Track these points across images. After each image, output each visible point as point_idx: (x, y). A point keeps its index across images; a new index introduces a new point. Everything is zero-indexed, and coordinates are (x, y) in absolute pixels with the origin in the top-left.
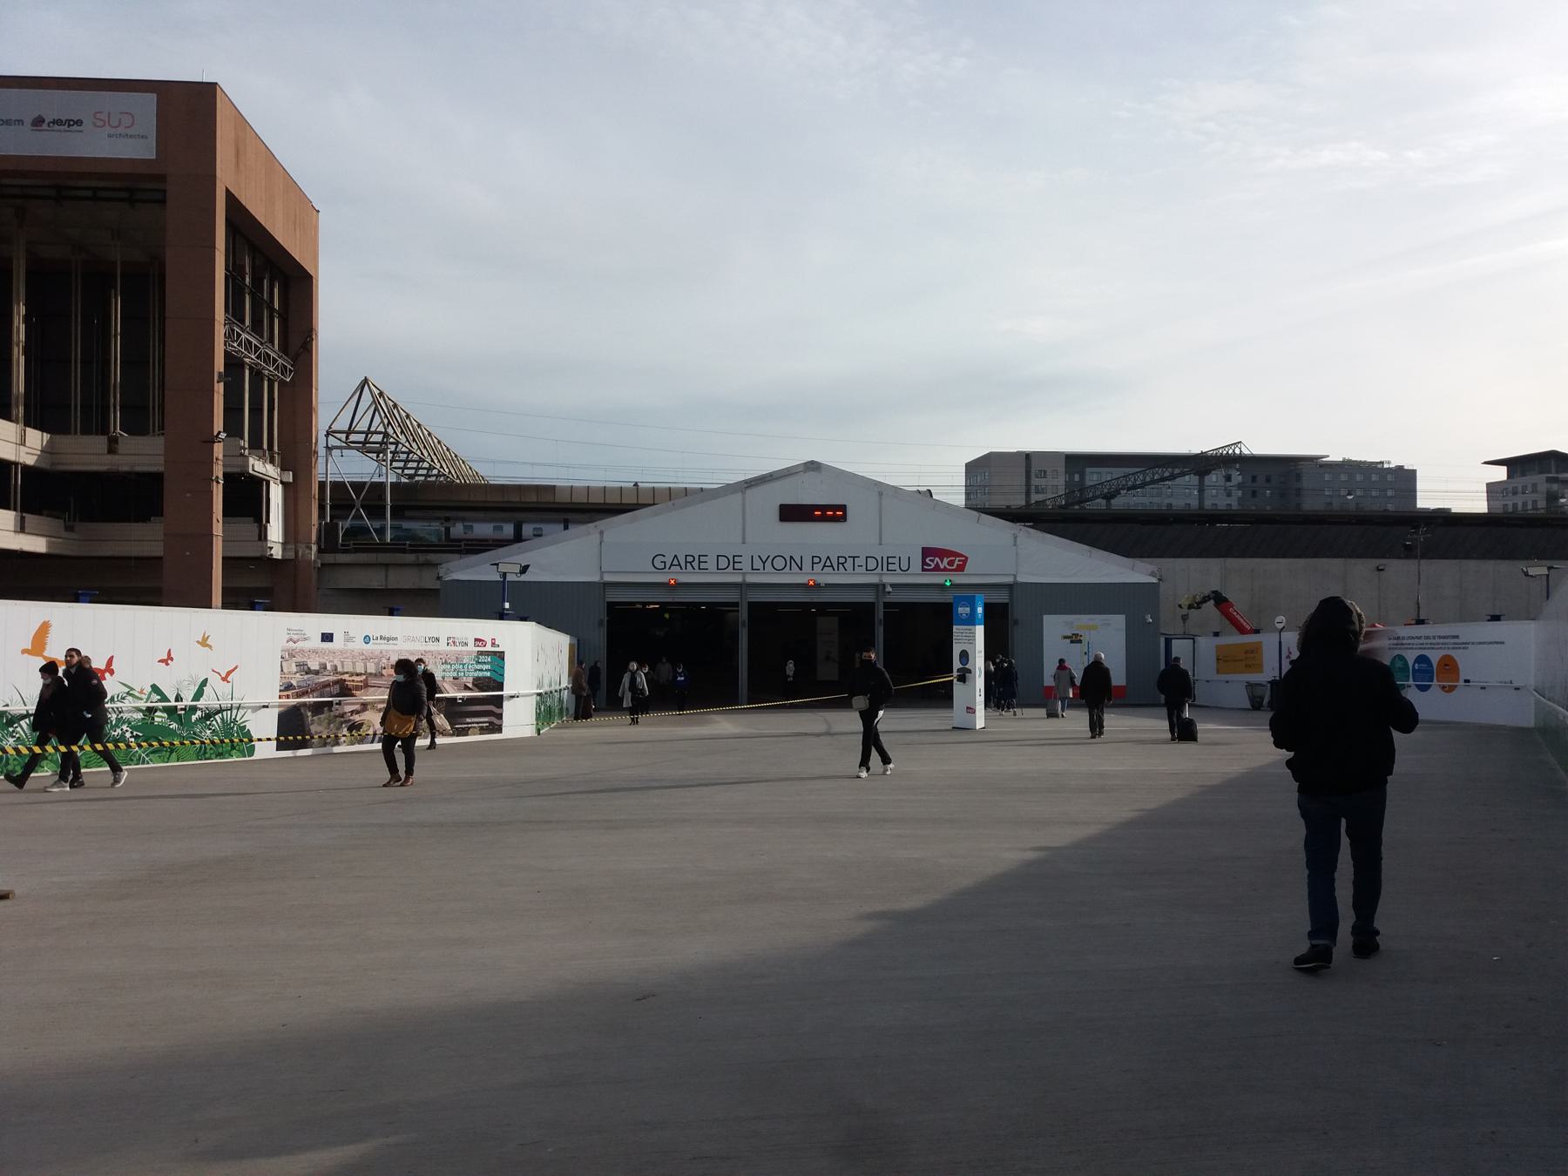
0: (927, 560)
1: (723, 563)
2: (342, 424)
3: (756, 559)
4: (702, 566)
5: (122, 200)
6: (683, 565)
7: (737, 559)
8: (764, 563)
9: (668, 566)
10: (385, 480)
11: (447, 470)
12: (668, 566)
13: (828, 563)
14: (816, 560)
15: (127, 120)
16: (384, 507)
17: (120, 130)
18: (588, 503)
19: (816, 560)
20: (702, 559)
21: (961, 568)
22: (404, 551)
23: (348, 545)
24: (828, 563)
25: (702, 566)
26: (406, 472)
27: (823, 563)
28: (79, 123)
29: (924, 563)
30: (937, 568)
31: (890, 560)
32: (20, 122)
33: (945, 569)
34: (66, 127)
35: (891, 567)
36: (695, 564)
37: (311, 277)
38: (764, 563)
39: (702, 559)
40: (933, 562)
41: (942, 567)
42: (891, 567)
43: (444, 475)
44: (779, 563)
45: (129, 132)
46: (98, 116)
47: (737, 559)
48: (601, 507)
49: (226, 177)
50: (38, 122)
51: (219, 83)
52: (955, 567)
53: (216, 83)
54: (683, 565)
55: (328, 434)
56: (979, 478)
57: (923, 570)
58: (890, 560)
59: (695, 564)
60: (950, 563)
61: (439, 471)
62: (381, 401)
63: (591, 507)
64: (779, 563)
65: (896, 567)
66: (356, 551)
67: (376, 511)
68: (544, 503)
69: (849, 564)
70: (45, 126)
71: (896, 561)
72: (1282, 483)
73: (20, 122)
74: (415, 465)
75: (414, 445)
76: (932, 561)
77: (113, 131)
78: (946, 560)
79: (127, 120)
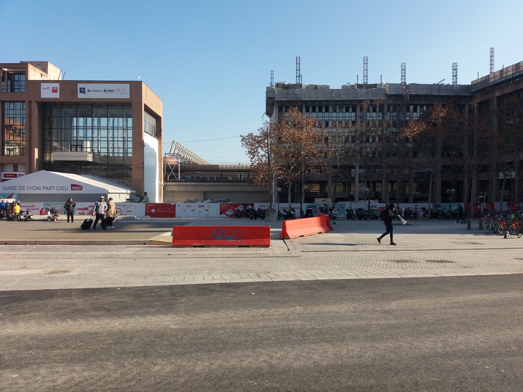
1: (20, 188)
2: (168, 152)
3: (29, 188)
4: (15, 189)
5: (121, 105)
6: (49, 189)
7: (24, 187)
14: (44, 187)
15: (123, 90)
16: (178, 171)
17: (122, 92)
19: (44, 187)
22: (183, 182)
25: (15, 189)
28: (113, 91)
29: (72, 188)
30: (75, 190)
32: (101, 91)
33: (77, 190)
35: (63, 189)
42: (63, 189)
44: (34, 188)
45: (124, 92)
47: (24, 187)
50: (105, 91)
54: (49, 189)
60: (78, 188)
62: (177, 145)
66: (172, 182)
67: (176, 171)
69: (52, 189)
70: (106, 92)
73: (101, 91)
78: (77, 187)
79: (123, 90)
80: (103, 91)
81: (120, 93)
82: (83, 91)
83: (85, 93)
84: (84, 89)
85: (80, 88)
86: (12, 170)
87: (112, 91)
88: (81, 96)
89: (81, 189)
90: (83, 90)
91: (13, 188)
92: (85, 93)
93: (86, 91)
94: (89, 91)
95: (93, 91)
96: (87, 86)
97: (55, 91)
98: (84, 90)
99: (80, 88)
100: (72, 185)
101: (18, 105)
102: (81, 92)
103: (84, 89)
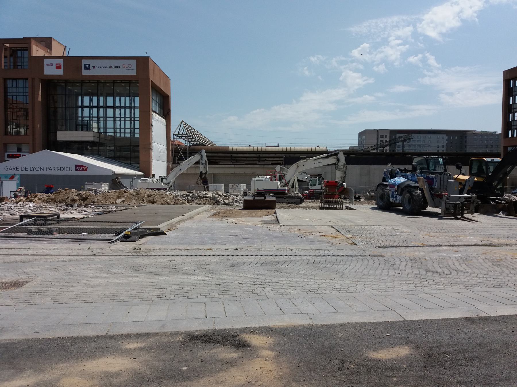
0: (77, 168)
2: (177, 133)
3: (31, 168)
4: (17, 169)
7: (26, 168)
8: (33, 169)
9: (9, 169)
10: (187, 145)
11: (200, 140)
12: (9, 169)
13: (50, 169)
18: (282, 152)
20: (17, 168)
21: (86, 170)
23: (179, 162)
24: (50, 169)
25: (17, 169)
26: (192, 142)
27: (49, 168)
28: (119, 67)
29: (76, 169)
30: (79, 170)
31: (67, 168)
33: (82, 171)
34: (117, 68)
35: (67, 170)
36: (16, 169)
37: (169, 96)
38: (33, 169)
39: (17, 168)
40: (78, 169)
41: (81, 170)
42: (67, 170)
43: (201, 143)
44: (37, 169)
45: (131, 69)
46: (123, 65)
47: (26, 168)
48: (290, 152)
49: (151, 78)
50: (111, 67)
51: (53, 37)
52: (84, 170)
53: (52, 38)
55: (174, 135)
56: (362, 142)
57: (76, 171)
58: (67, 168)
59: (16, 169)
60: (83, 169)
61: (200, 142)
63: (296, 152)
64: (37, 169)
65: (68, 170)
68: (221, 151)
69: (56, 169)
70: (112, 68)
71: (68, 168)
72: (456, 143)
74: (194, 141)
75: (191, 134)
76: (78, 168)
77: (127, 69)
78: (82, 168)
80: (108, 67)
81: (126, 70)
82: (87, 67)
83: (89, 69)
84: (89, 65)
85: (85, 65)
86: (16, 150)
87: (117, 67)
88: (85, 72)
89: (86, 170)
90: (88, 66)
91: (15, 168)
92: (89, 69)
93: (91, 67)
94: (94, 67)
95: (98, 67)
96: (92, 62)
97: (58, 67)
98: (89, 67)
99: (85, 65)
100: (77, 166)
101: (21, 83)
102: (86, 68)
103: (89, 65)
